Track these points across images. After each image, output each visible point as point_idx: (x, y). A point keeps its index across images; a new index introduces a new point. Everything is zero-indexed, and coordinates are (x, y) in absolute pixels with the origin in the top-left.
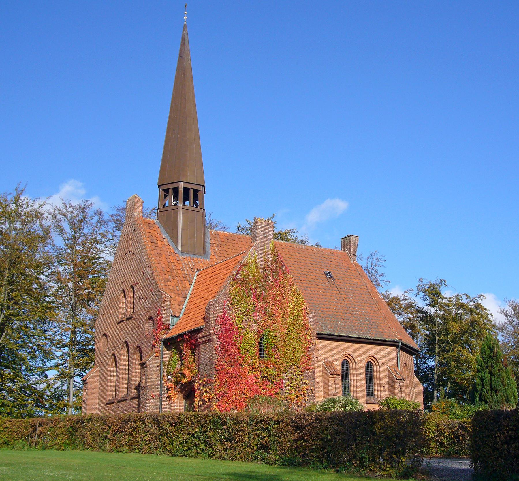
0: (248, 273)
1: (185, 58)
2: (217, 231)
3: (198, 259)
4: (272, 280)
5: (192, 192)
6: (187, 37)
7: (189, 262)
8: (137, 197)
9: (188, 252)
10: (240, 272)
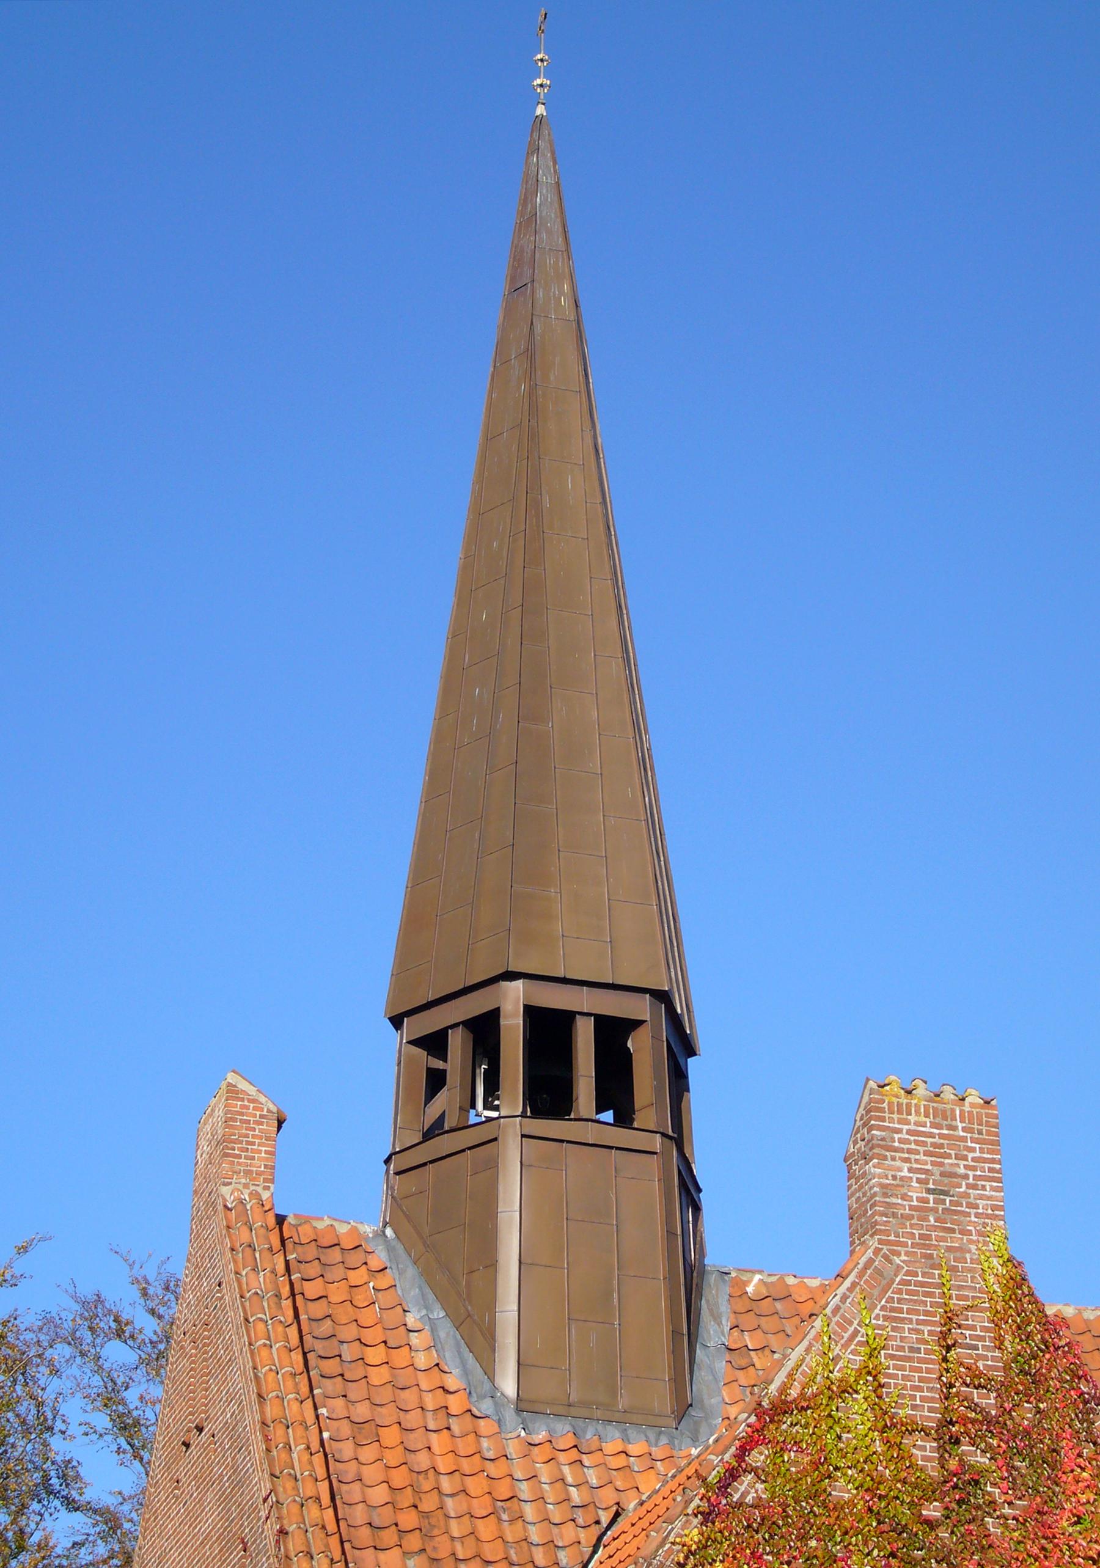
0: (816, 1465)
1: (540, 294)
2: (782, 1279)
3: (634, 1449)
4: (1007, 1510)
5: (584, 1036)
6: (551, 180)
7: (566, 1470)
8: (243, 1085)
9: (565, 1409)
10: (758, 1457)
